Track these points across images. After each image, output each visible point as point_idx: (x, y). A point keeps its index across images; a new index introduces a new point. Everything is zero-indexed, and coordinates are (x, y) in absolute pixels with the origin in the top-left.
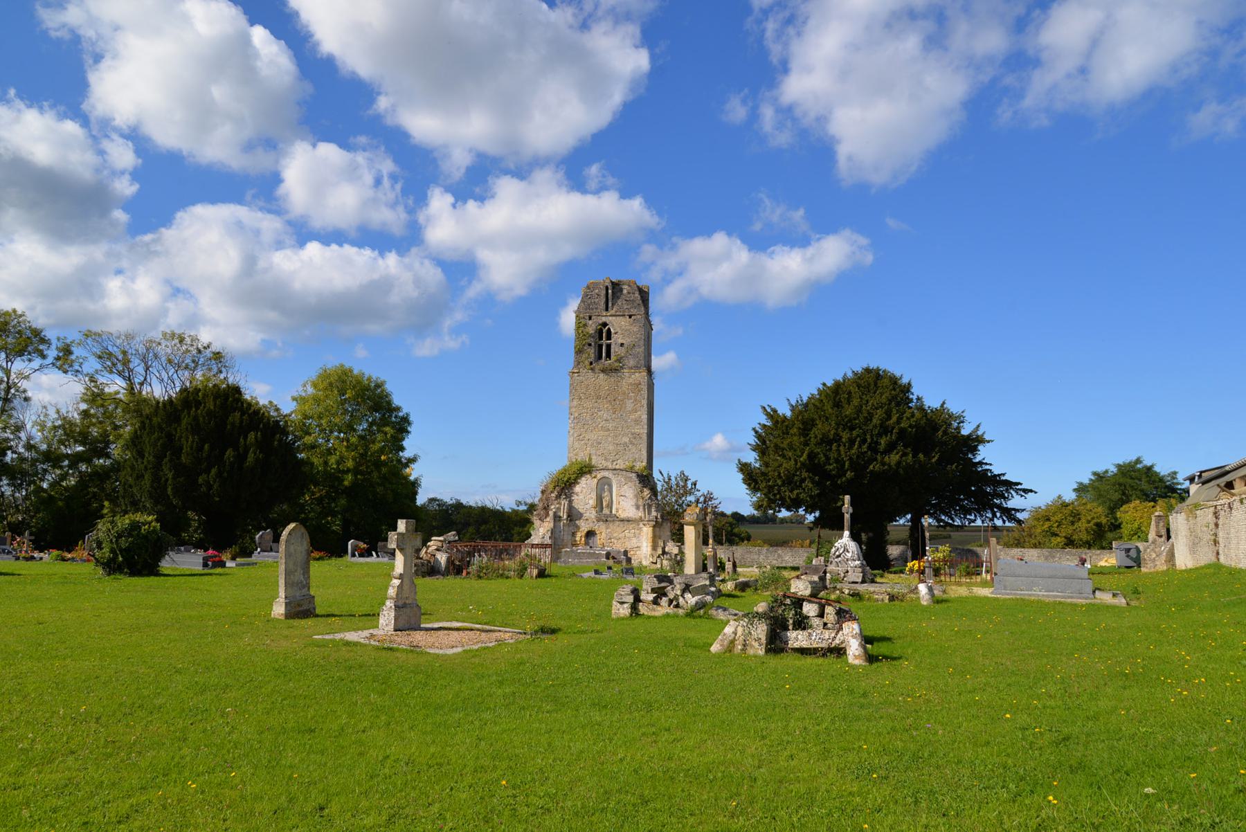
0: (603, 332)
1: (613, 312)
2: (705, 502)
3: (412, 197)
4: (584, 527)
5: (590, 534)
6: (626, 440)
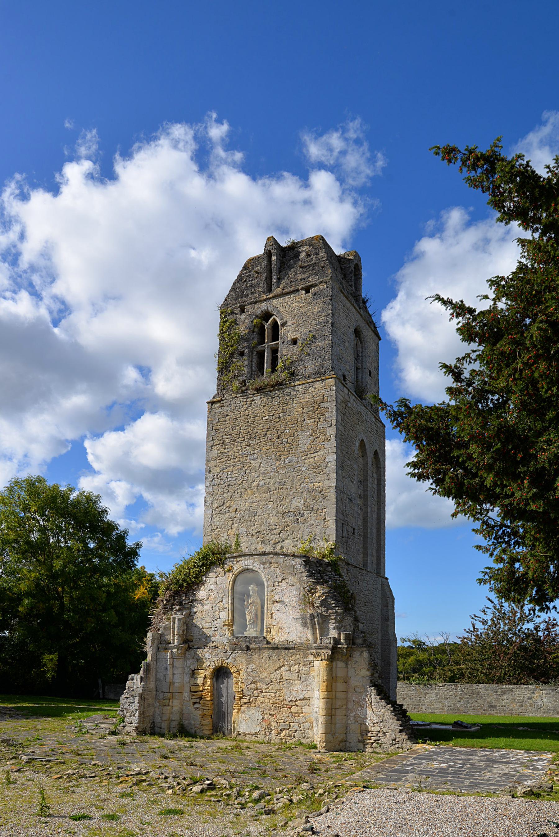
0: (266, 329)
1: (278, 291)
2: (547, 629)
3: (225, 127)
4: (210, 659)
5: (221, 673)
6: (298, 503)
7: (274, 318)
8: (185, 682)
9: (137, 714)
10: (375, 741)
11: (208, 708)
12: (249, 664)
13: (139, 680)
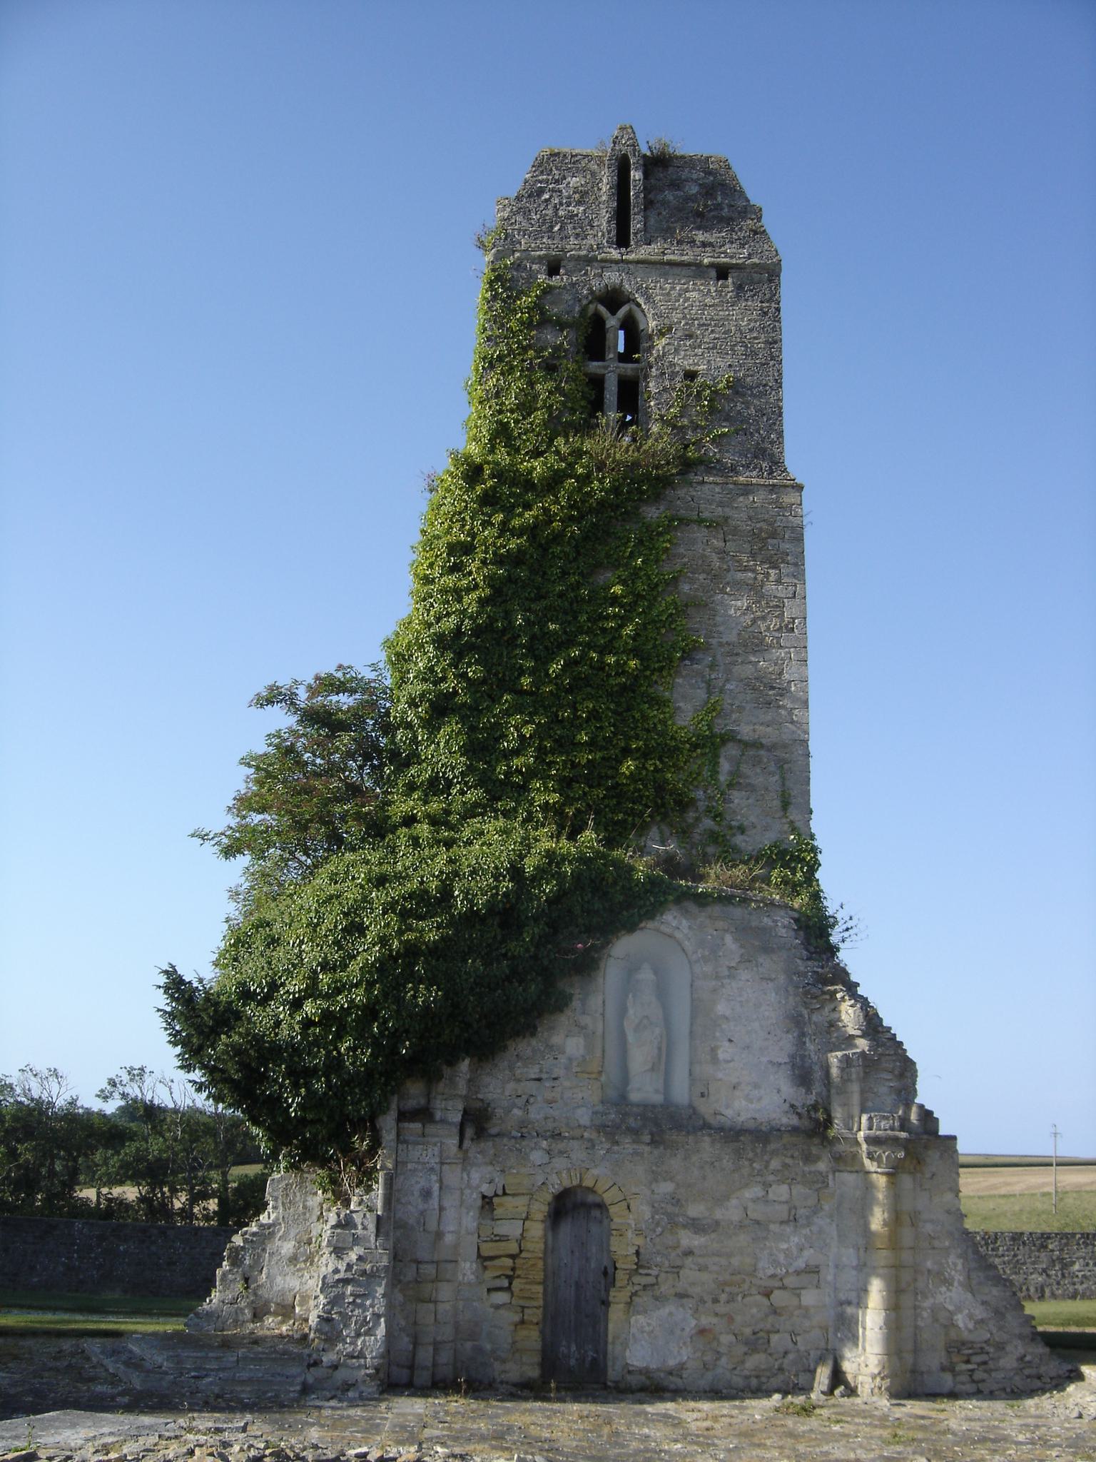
7: (630, 310)
8: (463, 1232)
9: (381, 1331)
10: (979, 1364)
11: (535, 1304)
12: (656, 1181)
13: (372, 1227)
